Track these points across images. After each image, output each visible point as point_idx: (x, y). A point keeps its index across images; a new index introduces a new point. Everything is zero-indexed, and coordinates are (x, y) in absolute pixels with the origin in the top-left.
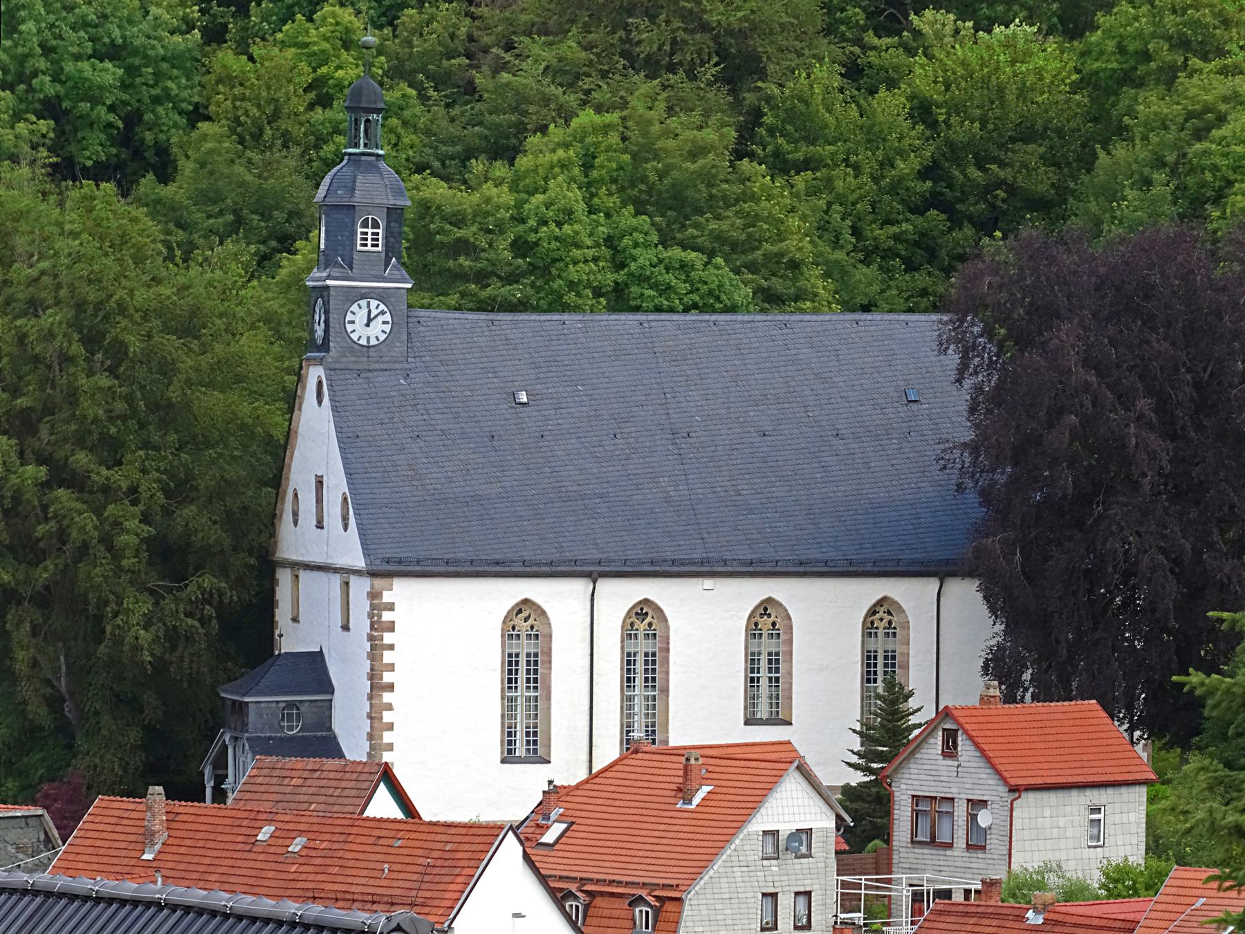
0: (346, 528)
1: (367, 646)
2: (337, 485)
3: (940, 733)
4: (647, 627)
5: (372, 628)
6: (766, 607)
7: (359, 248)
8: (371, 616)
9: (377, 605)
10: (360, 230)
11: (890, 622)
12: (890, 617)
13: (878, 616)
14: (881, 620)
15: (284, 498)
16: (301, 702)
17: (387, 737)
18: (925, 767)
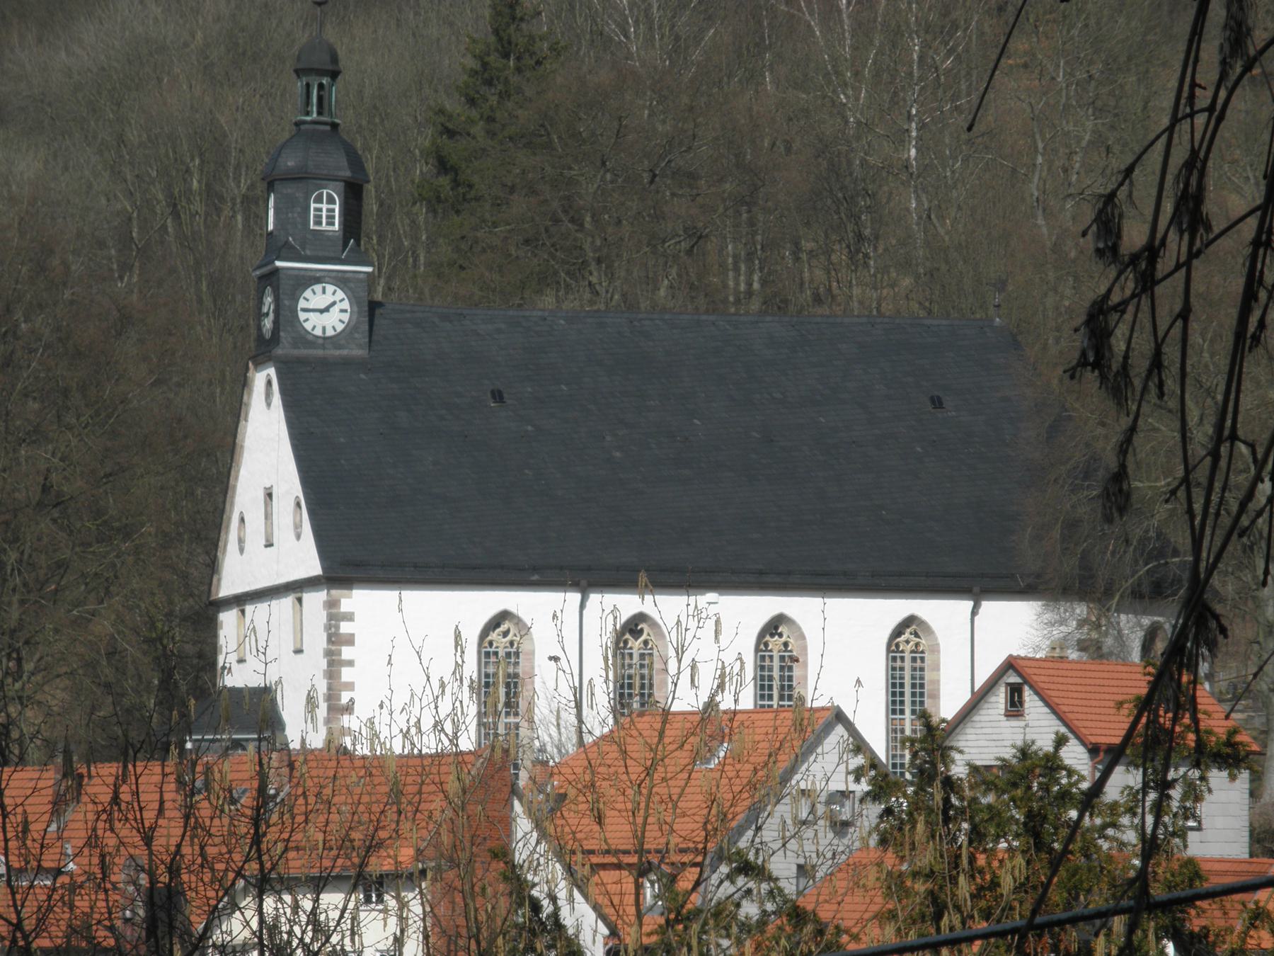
0: (298, 537)
1: (323, 664)
2: (289, 484)
3: (1003, 689)
4: (642, 645)
5: (330, 641)
6: (774, 626)
7: (312, 227)
8: (328, 627)
9: (335, 617)
10: (313, 206)
11: (917, 645)
12: (918, 640)
13: (903, 638)
14: (907, 642)
15: (228, 527)
16: (247, 740)
17: (346, 653)
18: (984, 731)
